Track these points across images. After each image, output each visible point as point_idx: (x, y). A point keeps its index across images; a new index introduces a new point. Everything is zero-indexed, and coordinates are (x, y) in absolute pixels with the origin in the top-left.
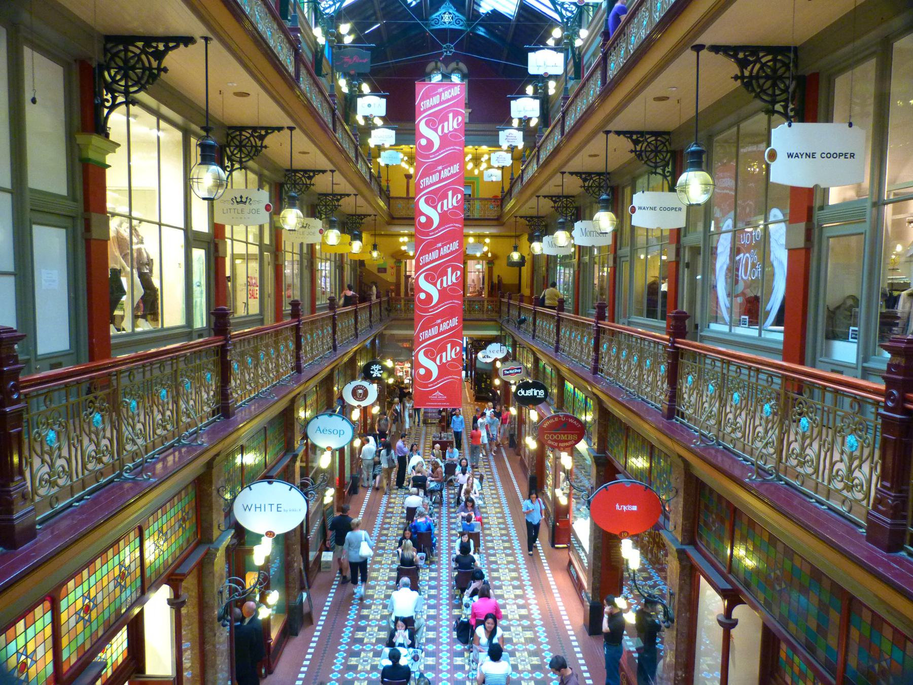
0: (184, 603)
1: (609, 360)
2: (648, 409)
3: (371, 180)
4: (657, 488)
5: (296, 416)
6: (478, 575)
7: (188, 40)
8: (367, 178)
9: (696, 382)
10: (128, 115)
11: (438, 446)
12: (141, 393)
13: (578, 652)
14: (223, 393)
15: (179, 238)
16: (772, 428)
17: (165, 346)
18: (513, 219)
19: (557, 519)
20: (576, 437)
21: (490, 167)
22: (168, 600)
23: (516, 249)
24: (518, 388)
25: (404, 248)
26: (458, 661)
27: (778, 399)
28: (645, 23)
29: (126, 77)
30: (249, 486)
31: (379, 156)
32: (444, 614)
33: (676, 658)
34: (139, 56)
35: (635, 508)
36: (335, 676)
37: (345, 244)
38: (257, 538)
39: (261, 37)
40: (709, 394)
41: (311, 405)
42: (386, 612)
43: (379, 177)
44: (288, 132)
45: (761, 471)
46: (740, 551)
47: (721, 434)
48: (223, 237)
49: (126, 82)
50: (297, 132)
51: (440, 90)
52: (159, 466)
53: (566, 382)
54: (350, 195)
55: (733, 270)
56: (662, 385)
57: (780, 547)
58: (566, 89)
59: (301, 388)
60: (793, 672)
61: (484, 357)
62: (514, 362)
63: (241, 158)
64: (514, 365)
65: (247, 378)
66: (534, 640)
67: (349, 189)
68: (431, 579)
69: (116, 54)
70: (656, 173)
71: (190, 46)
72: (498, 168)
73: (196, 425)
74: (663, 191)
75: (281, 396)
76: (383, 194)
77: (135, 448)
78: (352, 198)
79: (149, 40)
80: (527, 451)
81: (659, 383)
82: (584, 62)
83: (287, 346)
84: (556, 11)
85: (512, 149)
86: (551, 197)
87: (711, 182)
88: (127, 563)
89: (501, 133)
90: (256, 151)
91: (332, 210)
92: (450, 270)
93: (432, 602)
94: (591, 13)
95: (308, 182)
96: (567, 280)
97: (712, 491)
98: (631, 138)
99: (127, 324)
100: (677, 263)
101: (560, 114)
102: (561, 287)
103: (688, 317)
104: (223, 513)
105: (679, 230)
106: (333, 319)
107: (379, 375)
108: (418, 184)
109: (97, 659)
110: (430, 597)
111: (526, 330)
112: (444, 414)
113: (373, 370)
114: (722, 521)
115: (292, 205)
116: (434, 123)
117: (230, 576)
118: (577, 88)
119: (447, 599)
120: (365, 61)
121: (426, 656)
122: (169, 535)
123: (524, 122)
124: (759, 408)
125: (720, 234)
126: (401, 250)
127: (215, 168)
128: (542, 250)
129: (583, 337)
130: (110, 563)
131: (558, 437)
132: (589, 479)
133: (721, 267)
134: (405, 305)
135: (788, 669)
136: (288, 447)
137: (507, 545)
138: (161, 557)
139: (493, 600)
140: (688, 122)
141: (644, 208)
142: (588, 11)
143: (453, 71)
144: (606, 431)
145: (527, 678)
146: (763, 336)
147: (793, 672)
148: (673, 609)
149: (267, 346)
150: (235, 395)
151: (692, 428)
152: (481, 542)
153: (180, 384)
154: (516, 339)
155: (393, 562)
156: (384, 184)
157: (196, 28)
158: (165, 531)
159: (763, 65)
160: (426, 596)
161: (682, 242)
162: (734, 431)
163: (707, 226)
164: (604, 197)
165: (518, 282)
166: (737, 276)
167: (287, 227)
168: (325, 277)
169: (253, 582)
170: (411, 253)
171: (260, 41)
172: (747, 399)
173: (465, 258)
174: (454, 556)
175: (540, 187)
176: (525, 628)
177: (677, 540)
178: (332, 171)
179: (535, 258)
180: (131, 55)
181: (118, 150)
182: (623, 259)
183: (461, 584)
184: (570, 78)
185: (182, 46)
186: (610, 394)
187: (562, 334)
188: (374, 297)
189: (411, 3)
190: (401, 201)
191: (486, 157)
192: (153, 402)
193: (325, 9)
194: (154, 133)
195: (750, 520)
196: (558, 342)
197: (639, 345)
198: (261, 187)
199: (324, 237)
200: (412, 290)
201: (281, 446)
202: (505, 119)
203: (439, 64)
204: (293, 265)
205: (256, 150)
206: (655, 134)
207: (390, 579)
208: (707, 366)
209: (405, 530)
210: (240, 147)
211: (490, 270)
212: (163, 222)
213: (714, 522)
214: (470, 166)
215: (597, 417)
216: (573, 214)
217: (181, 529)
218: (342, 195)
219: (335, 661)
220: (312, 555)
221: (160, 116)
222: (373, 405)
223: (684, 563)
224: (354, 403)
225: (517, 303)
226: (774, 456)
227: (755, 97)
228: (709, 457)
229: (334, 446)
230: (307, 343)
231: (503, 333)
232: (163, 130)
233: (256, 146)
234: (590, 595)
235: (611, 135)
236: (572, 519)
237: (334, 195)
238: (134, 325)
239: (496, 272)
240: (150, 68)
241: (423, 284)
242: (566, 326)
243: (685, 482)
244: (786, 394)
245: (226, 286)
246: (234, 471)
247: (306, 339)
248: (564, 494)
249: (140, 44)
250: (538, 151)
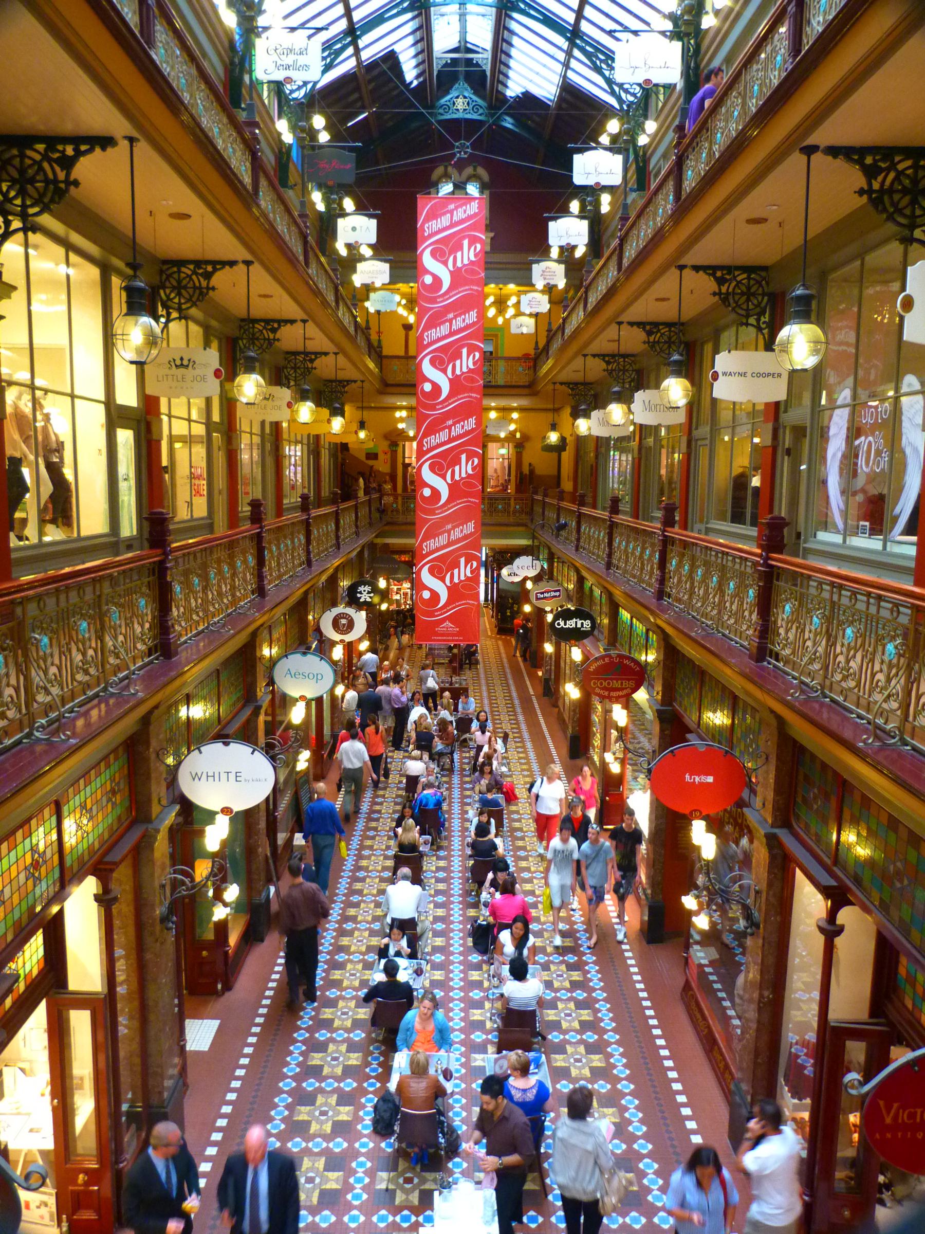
0: (115, 899)
1: (680, 581)
2: (730, 648)
3: (356, 331)
4: (742, 753)
5: (258, 654)
6: (501, 865)
7: (106, 142)
8: (352, 330)
9: (796, 612)
10: (26, 245)
11: (447, 694)
12: (55, 626)
13: (636, 974)
14: (162, 626)
15: (99, 414)
16: (897, 674)
17: (83, 563)
18: (551, 387)
20: (632, 684)
21: (519, 314)
22: (95, 895)
23: (554, 427)
24: (556, 618)
25: (401, 426)
26: (475, 976)
27: (905, 636)
28: (736, 113)
29: (22, 193)
30: (199, 749)
31: (368, 299)
33: (762, 973)
34: (39, 163)
35: (710, 779)
36: (286, 1085)
38: (210, 816)
39: (207, 136)
40: (813, 628)
41: (279, 640)
42: (379, 912)
43: (368, 328)
44: (242, 267)
45: (879, 732)
46: (850, 836)
47: (828, 683)
48: (158, 414)
49: (23, 201)
50: (256, 268)
51: (452, 206)
52: (80, 723)
55: (850, 456)
56: (750, 615)
57: (904, 834)
58: (625, 206)
59: (265, 618)
60: (915, 993)
61: (510, 575)
62: (551, 582)
63: (180, 304)
64: (551, 586)
65: (193, 604)
67: (327, 346)
68: (439, 869)
69: (9, 161)
70: (747, 324)
71: (109, 150)
72: (531, 315)
73: (128, 669)
74: (756, 350)
75: (239, 628)
77: (49, 698)
78: (331, 357)
79: (52, 141)
80: (567, 701)
81: (746, 613)
82: (651, 167)
83: (245, 562)
84: (613, 93)
85: (549, 289)
86: (602, 356)
87: (823, 339)
88: (41, 847)
89: (535, 266)
90: (201, 295)
91: (304, 375)
92: (464, 457)
93: (440, 899)
94: (661, 97)
95: (204, 283)
96: (622, 469)
97: (813, 757)
98: (713, 275)
99: (31, 531)
100: (774, 448)
101: (617, 241)
102: (616, 480)
103: (787, 524)
104: (164, 784)
105: (777, 404)
106: (307, 526)
107: (369, 600)
108: (420, 339)
109: (7, 971)
110: (438, 892)
111: (567, 539)
112: (455, 651)
114: (827, 797)
115: (250, 370)
116: (443, 254)
117: (174, 865)
118: (641, 203)
119: (460, 895)
120: (347, 167)
121: (433, 968)
122: (94, 813)
123: (567, 251)
124: (880, 648)
125: (834, 409)
126: (397, 429)
127: (146, 320)
128: (590, 429)
129: (644, 549)
130: (20, 848)
132: (650, 739)
133: (834, 455)
134: (403, 503)
135: (908, 990)
136: (249, 696)
138: (85, 841)
139: (520, 896)
140: (794, 252)
142: (657, 94)
143: (469, 179)
144: (673, 676)
146: (888, 549)
147: (915, 993)
148: (759, 910)
149: (219, 561)
150: (177, 628)
151: (788, 674)
152: (505, 821)
153: (105, 614)
154: (553, 550)
155: (388, 848)
156: (374, 337)
157: (118, 125)
158: (89, 806)
159: (900, 174)
160: (432, 892)
161: (781, 420)
162: (845, 678)
163: (816, 398)
164: (676, 357)
165: (556, 473)
166: (856, 464)
167: (244, 400)
168: (295, 465)
169: (205, 873)
170: (411, 433)
171: (204, 142)
172: (863, 636)
173: (482, 439)
174: (469, 840)
175: (587, 344)
176: (580, 1005)
177: (766, 821)
178: (304, 321)
179: (580, 441)
180: (183, 275)
181: (14, 295)
182: (699, 443)
183: (477, 878)
184: (632, 190)
185: (98, 150)
186: (681, 627)
187: (616, 544)
188: (361, 493)
189: (411, 83)
190: (396, 361)
191: (513, 300)
192: (71, 638)
193: (292, 92)
194: (62, 269)
195: (864, 797)
196: (610, 555)
197: (719, 561)
198: (207, 344)
199: (294, 413)
200: (412, 482)
201: (238, 695)
202: (540, 247)
203: (450, 169)
204: (252, 449)
205: (201, 293)
206: (748, 269)
207: (385, 869)
209: (404, 807)
210: (179, 288)
211: (519, 456)
212: (76, 393)
213: (815, 798)
214: (491, 312)
215: (661, 657)
216: (633, 380)
217: (110, 805)
218: (318, 354)
219: (288, 1059)
220: (281, 837)
221: (69, 247)
222: (360, 640)
223: (775, 851)
224: (336, 637)
225: (555, 502)
226: (899, 713)
227: (888, 219)
228: (810, 713)
229: (309, 695)
230: (272, 557)
231: (536, 543)
232: (74, 266)
233: (200, 288)
234: (649, 891)
235: (686, 272)
236: (626, 793)
237: (306, 354)
238: (41, 533)
239: (527, 459)
240: (56, 181)
241: (427, 475)
242: (621, 535)
243: (779, 746)
244: (916, 630)
245: (162, 480)
246: (178, 727)
247: (271, 551)
248: (616, 759)
249: (41, 147)
250: (586, 292)
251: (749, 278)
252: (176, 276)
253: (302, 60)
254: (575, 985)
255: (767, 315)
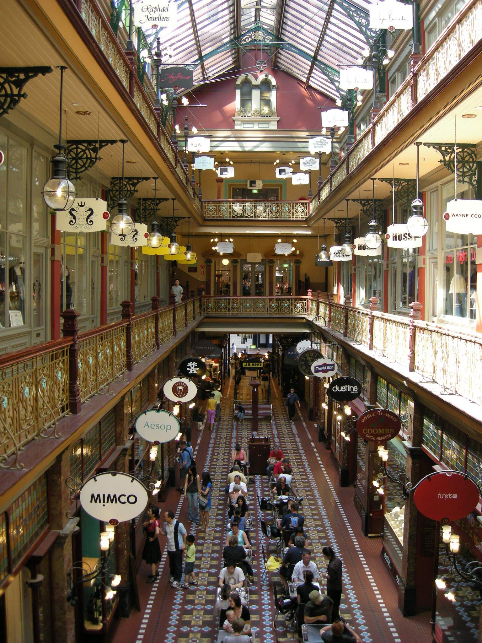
19: (370, 510)
32: (266, 599)
35: (455, 496)
37: (182, 253)
44: (120, 144)
53: (379, 377)
71: (47, 75)
76: (196, 196)
95: (132, 189)
113: (189, 367)
131: (375, 431)
134: (216, 303)
137: (322, 534)
141: (457, 215)
159: (403, 187)
165: (324, 281)
211: (297, 269)
224: (175, 399)
235: (421, 147)
252: (75, 151)
253: (164, 14)
255: (476, 176)
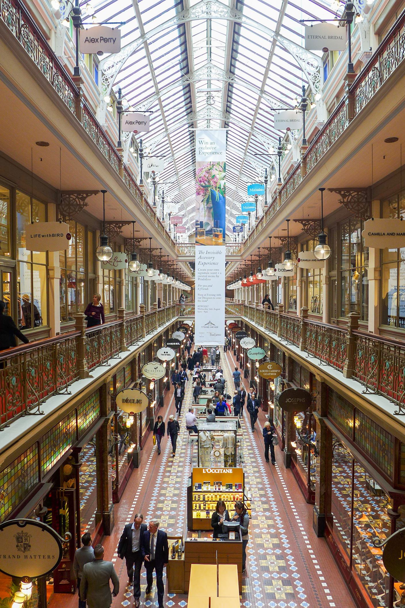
1: (311, 341)
54: (147, 238)
66: (274, 526)
145: (275, 573)
159: (353, 197)
208: (385, 350)
251: (315, 223)
254: (269, 527)
